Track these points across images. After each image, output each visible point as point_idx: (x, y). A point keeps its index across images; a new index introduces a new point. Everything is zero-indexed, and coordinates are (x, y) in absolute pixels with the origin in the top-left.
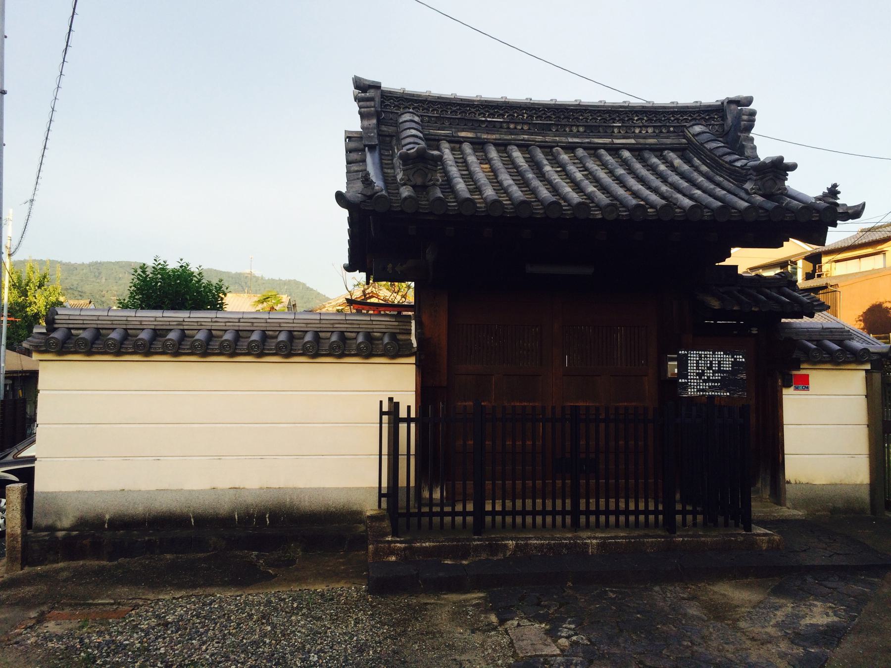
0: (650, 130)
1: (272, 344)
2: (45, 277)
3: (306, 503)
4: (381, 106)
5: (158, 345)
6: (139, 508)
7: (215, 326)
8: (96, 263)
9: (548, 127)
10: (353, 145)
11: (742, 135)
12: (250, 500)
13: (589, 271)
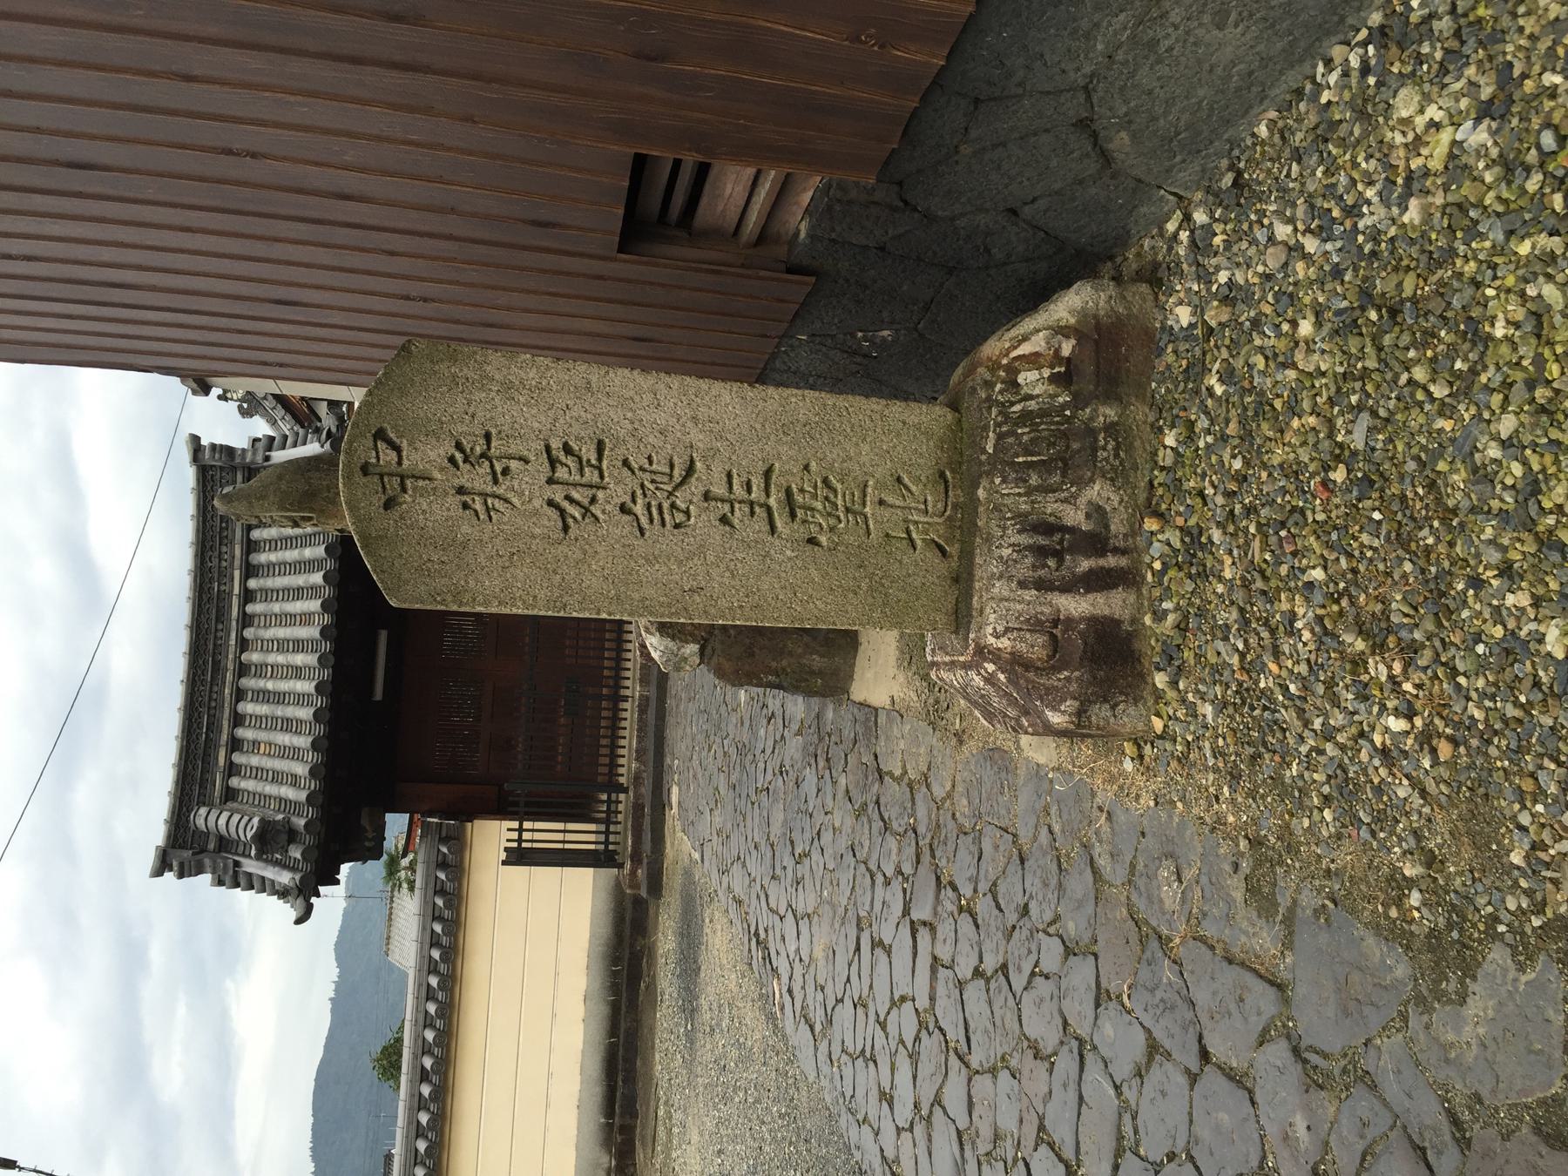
0: (224, 549)
1: (449, 886)
3: (605, 930)
4: (185, 849)
6: (597, 1091)
9: (216, 664)
10: (228, 879)
11: (238, 460)
12: (597, 985)
13: (383, 635)
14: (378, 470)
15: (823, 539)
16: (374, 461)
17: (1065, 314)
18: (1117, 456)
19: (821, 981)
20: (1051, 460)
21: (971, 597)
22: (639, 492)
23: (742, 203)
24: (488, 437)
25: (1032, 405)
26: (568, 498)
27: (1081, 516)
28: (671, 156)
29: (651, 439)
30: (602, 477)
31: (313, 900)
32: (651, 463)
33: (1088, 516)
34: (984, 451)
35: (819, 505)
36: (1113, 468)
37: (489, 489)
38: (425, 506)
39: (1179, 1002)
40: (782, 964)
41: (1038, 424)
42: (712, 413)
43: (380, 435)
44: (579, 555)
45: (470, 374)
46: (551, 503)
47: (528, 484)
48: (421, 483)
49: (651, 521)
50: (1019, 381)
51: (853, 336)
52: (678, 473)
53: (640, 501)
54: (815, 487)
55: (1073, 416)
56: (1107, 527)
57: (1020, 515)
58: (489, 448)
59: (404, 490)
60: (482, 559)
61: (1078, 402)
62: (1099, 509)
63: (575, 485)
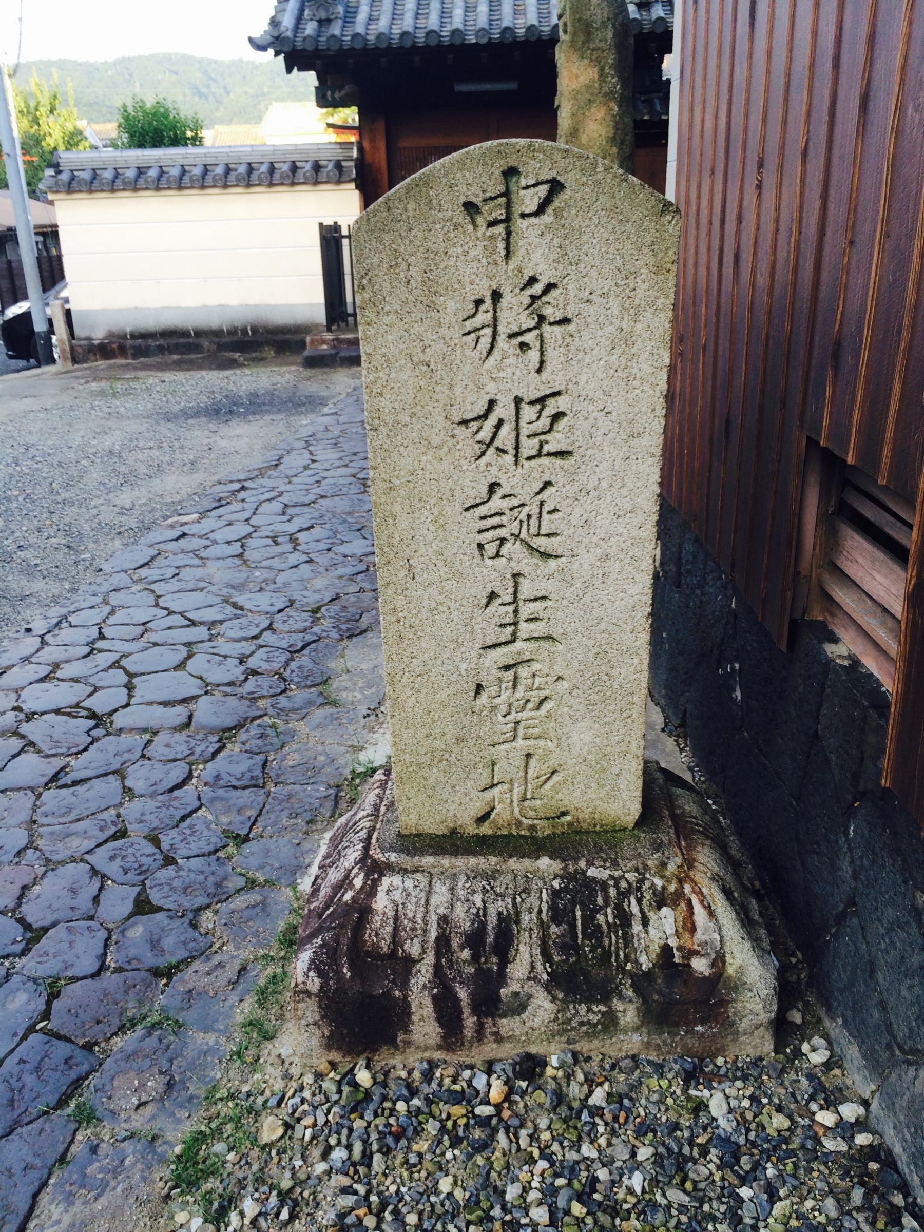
1: (232, 176)
2: (55, 97)
5: (141, 182)
7: (185, 162)
8: (123, 59)
13: (513, 86)
14: (513, 188)
15: (484, 698)
16: (523, 182)
17: (738, 962)
18: (582, 1024)
19: (184, 573)
20: (577, 948)
21: (434, 854)
22: (515, 502)
23: (866, 588)
24: (565, 321)
25: (637, 928)
26: (501, 422)
27: (515, 987)
28: (916, 521)
29: (578, 511)
30: (529, 458)
31: (271, 52)
32: (549, 512)
33: (516, 994)
34: (590, 864)
35: (520, 693)
36: (569, 1021)
37: (501, 329)
38: (473, 253)
39: (16, 1113)
40: (208, 524)
41: (616, 932)
42: (614, 575)
43: (556, 187)
44: (436, 441)
45: (640, 293)
46: (492, 403)
47: (513, 376)
48: (501, 245)
49: (483, 518)
50: (664, 909)
51: (736, 659)
52: (541, 543)
53: (506, 504)
54: (539, 689)
55: (624, 972)
56: (504, 1015)
57: (518, 914)
58: (551, 324)
59: (491, 224)
60: (417, 328)
61: (642, 981)
62: (523, 1008)
63: (517, 428)
